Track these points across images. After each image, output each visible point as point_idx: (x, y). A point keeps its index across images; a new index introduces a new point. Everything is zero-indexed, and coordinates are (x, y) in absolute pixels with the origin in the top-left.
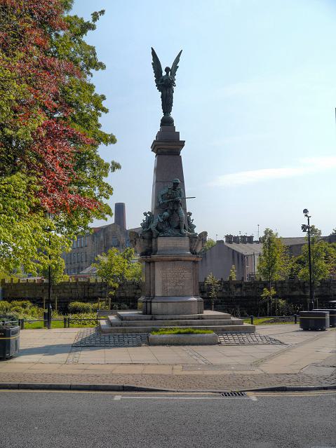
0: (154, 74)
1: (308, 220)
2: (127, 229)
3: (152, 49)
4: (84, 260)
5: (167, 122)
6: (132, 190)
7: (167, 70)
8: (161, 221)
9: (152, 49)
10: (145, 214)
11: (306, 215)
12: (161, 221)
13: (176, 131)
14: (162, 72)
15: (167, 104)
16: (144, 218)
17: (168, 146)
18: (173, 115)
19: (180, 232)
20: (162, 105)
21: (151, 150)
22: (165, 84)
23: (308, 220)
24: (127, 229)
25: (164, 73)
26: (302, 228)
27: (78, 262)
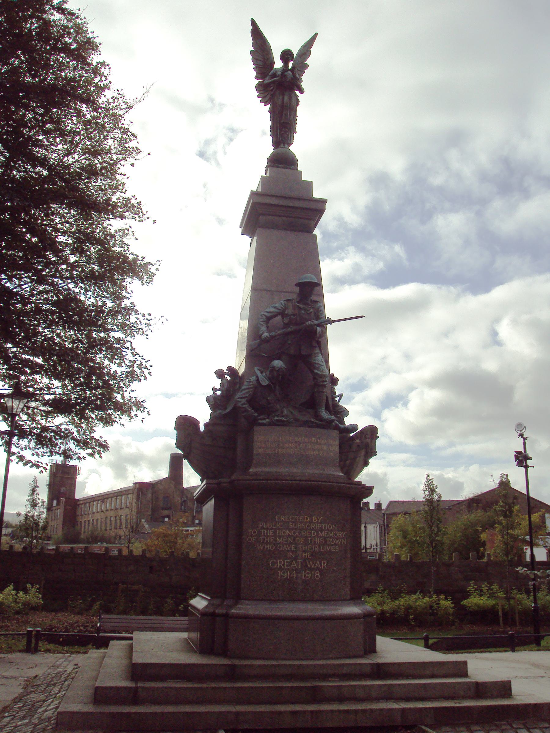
0: (254, 73)
1: (524, 444)
2: (185, 486)
3: (253, 22)
4: (108, 528)
5: (282, 161)
6: (185, 336)
7: (286, 55)
8: (265, 383)
9: (253, 22)
10: (220, 374)
11: (521, 435)
12: (265, 383)
13: (304, 178)
14: (273, 63)
15: (283, 127)
16: (217, 383)
17: (283, 213)
18: (298, 147)
19: (317, 416)
20: (272, 128)
21: (240, 230)
22: (280, 85)
23: (524, 444)
24: (185, 486)
25: (278, 64)
26: (516, 457)
27: (116, 528)
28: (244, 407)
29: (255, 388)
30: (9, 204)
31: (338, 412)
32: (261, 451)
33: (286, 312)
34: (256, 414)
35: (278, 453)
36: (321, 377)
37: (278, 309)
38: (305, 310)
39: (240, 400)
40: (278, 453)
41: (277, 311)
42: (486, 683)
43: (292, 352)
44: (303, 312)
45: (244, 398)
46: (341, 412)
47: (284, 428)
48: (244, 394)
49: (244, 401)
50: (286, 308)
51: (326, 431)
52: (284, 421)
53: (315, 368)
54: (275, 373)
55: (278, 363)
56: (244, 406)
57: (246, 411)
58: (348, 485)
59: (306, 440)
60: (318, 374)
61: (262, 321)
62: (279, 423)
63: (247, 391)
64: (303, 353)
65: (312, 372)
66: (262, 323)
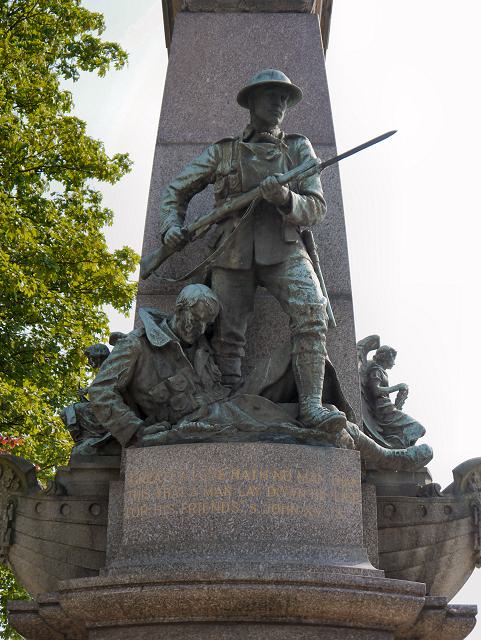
28: (107, 406)
29: (137, 355)
31: (394, 428)
33: (219, 169)
34: (139, 422)
35: (186, 515)
37: (203, 166)
38: (260, 154)
39: (99, 388)
40: (186, 515)
41: (200, 170)
43: (234, 262)
45: (108, 382)
46: (402, 428)
48: (109, 373)
49: (109, 390)
51: (321, 452)
52: (202, 430)
53: (289, 293)
54: (189, 316)
55: (194, 292)
56: (110, 402)
58: (113, 592)
60: (298, 307)
61: (168, 204)
64: (261, 260)
65: (284, 304)
66: (168, 207)
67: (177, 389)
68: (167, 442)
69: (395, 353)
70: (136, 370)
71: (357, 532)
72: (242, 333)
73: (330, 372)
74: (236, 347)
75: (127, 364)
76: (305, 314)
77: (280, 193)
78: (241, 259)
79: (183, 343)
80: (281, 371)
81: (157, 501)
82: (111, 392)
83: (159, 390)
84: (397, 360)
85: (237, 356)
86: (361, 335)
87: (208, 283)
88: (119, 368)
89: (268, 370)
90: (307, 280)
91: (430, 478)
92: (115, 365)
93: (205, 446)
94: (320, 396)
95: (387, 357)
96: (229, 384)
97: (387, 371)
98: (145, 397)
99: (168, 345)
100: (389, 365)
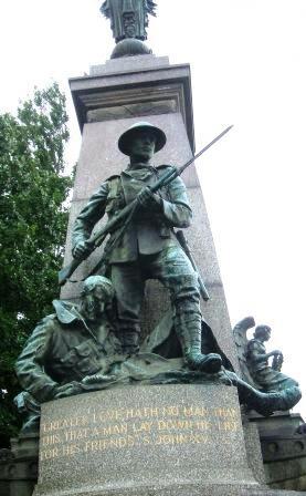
30: (5, 391)
32: (54, 453)
34: (54, 384)
35: (89, 451)
36: (180, 283)
40: (89, 451)
42: (82, 152)
44: (133, 180)
47: (100, 394)
50: (108, 190)
54: (90, 299)
57: (33, 379)
59: (155, 411)
62: (92, 387)
63: (38, 339)
67: (83, 354)
68: (74, 393)
69: (269, 330)
70: (51, 343)
71: (239, 455)
72: (136, 312)
73: (207, 330)
74: (133, 323)
75: (43, 341)
76: (180, 283)
77: (153, 199)
78: (129, 256)
79: (88, 321)
80: (166, 334)
81: (65, 443)
82: (32, 363)
83: (69, 356)
84: (272, 334)
85: (134, 330)
86: (235, 319)
87: (107, 275)
88: (38, 343)
89: (158, 336)
90: (181, 260)
91: (156, 150)
92: (34, 342)
93: (103, 392)
94: (200, 347)
95: (263, 334)
96: (127, 349)
97: (265, 343)
98: (58, 366)
99: (76, 321)
100: (266, 339)
